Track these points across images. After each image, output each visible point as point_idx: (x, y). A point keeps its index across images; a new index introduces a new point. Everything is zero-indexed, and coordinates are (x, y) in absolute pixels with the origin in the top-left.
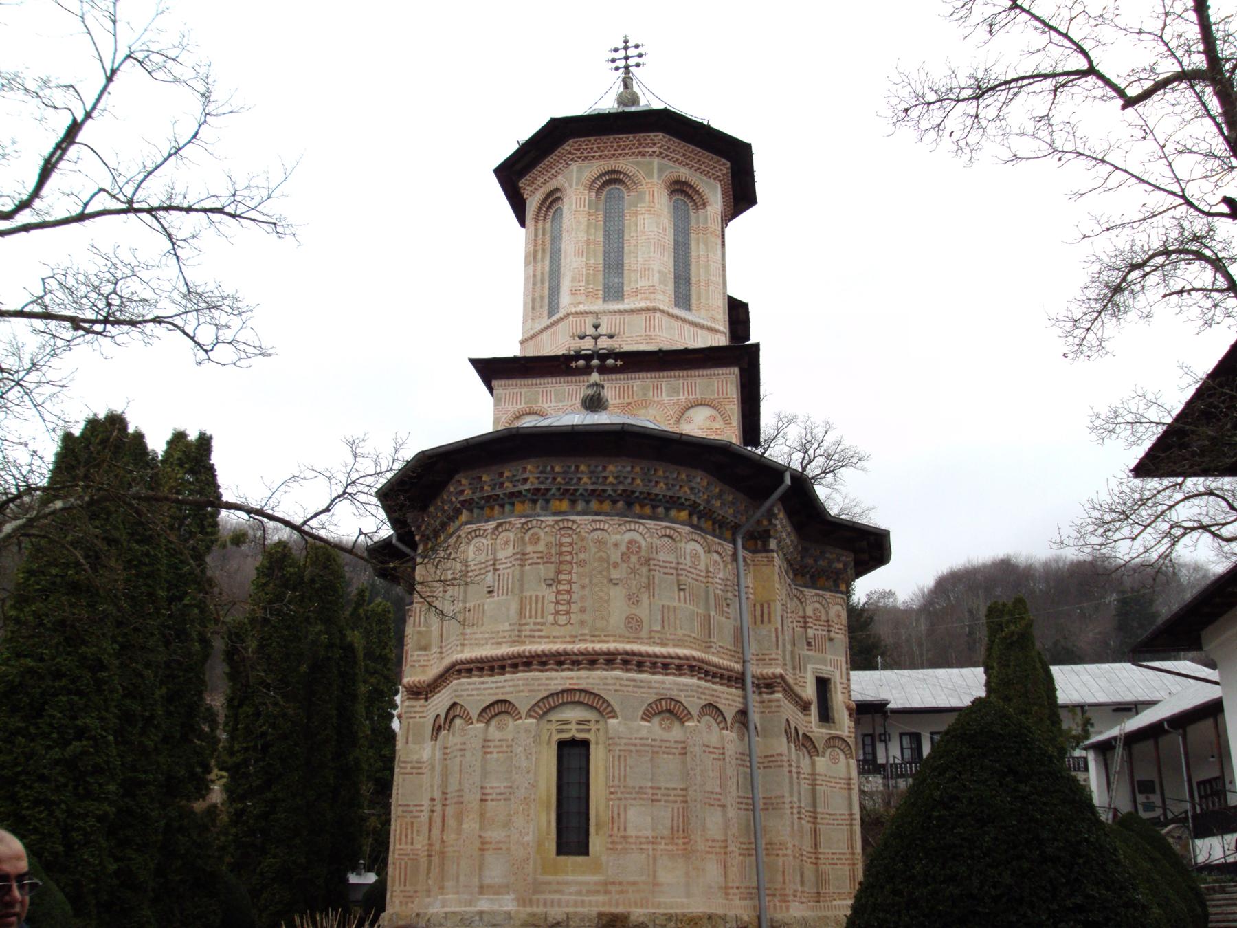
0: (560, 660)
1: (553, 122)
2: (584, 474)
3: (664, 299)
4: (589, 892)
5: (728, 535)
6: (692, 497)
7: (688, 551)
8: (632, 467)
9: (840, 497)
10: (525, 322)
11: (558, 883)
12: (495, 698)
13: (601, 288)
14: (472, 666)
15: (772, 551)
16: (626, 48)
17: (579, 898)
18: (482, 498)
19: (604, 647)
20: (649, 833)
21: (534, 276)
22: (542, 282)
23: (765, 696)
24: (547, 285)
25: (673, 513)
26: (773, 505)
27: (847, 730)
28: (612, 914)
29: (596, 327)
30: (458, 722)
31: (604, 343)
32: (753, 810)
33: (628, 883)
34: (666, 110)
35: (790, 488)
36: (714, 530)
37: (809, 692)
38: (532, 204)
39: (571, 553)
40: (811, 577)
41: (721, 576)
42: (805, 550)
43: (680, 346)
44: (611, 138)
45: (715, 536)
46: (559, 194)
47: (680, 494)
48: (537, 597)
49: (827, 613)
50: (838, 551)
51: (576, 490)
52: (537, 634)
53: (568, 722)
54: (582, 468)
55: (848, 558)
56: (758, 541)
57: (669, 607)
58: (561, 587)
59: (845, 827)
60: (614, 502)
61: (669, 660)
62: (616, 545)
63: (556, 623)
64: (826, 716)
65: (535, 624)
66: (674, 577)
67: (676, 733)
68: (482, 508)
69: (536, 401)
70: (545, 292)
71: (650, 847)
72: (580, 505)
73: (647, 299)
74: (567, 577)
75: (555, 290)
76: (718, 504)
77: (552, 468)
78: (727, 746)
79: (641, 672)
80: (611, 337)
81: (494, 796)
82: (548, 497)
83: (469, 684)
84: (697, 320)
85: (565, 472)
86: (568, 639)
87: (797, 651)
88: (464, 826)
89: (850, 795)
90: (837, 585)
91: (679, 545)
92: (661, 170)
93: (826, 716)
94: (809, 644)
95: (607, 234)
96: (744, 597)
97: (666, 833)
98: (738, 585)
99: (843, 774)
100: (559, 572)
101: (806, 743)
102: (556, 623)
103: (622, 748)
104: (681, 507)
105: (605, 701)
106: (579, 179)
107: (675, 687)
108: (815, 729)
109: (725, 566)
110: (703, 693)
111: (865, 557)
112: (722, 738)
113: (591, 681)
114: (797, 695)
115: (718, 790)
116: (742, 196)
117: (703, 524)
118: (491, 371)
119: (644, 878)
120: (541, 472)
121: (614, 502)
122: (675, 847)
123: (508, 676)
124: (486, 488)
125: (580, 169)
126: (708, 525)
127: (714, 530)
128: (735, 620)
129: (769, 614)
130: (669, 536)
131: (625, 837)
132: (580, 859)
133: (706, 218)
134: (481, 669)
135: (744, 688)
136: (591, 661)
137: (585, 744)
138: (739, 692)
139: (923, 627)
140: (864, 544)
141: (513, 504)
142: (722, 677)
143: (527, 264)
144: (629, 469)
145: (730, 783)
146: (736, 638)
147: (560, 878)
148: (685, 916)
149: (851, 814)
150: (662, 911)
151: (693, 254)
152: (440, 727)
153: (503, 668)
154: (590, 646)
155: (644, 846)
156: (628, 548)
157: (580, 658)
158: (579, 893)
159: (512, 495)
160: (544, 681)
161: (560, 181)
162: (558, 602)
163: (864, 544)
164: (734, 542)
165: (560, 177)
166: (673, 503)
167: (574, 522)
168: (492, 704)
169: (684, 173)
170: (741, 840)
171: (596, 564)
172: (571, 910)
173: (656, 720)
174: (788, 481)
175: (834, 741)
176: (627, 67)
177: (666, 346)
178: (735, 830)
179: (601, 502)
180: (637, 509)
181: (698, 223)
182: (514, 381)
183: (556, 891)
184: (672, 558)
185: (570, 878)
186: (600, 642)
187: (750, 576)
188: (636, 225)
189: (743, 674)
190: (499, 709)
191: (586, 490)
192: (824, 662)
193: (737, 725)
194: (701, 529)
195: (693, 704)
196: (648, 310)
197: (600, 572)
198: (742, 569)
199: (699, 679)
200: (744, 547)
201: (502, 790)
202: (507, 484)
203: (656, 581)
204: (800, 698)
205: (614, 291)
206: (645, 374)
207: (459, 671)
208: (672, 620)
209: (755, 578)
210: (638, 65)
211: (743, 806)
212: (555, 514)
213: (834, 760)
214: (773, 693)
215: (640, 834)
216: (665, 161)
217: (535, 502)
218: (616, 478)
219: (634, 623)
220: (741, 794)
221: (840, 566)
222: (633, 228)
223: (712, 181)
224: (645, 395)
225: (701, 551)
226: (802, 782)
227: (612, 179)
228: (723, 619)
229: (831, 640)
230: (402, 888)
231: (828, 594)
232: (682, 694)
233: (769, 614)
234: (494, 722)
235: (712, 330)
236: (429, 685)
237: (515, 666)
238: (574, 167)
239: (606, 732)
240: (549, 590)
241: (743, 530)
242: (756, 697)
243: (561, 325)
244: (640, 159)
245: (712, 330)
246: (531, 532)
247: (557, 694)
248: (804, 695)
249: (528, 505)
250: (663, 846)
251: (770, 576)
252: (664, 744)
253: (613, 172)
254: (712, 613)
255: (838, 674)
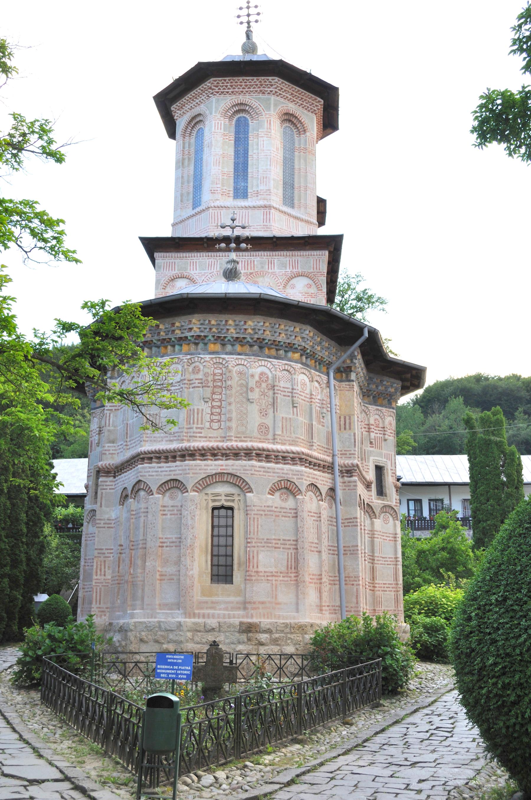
0: (214, 453)
1: (200, 64)
2: (232, 324)
3: (276, 199)
4: (233, 609)
5: (324, 369)
6: (303, 344)
7: (299, 380)
8: (264, 323)
9: (45, 155)
10: (175, 210)
11: (213, 602)
12: (169, 478)
13: (232, 189)
14: (152, 455)
15: (353, 381)
16: (248, 8)
17: (227, 612)
18: (159, 340)
19: (244, 445)
20: (273, 569)
21: (182, 177)
22: (188, 182)
23: (346, 479)
24: (191, 184)
25: (290, 354)
26: (355, 350)
27: (394, 501)
28: (250, 624)
29: (233, 220)
30: (142, 493)
31: (238, 232)
32: (338, 555)
33: (259, 602)
34: (281, 61)
35: (367, 340)
36: (315, 366)
37: (371, 476)
38: (181, 124)
39: (221, 380)
40: (374, 397)
41: (319, 397)
42: (370, 379)
43: (289, 235)
44: (241, 79)
45: (316, 370)
46: (201, 118)
47: (296, 342)
48: (198, 409)
49: (383, 422)
50: (392, 380)
51: (225, 337)
52: (198, 435)
53: (218, 495)
54: (230, 322)
55: (398, 384)
56: (344, 373)
57: (286, 418)
58: (214, 404)
59: (392, 566)
60: (251, 346)
61: (286, 454)
62: (252, 376)
63: (211, 428)
64: (381, 492)
65: (197, 428)
66: (290, 398)
67: (290, 503)
68: (158, 347)
69: (186, 269)
70: (191, 188)
71: (274, 578)
72: (229, 348)
73: (264, 199)
74: (219, 397)
75: (198, 188)
76: (319, 348)
77: (210, 321)
78: (322, 512)
79: (268, 462)
80: (244, 228)
81: (168, 544)
82: (206, 341)
83: (150, 468)
84: (299, 215)
85: (219, 324)
86: (219, 439)
87: (364, 448)
88: (147, 564)
89: (396, 545)
90: (390, 403)
91: (294, 376)
92: (276, 105)
93: (381, 492)
94: (371, 443)
95: (236, 152)
96: (334, 411)
97: (284, 569)
98: (330, 404)
99: (391, 531)
100: (213, 393)
101: (369, 509)
102: (211, 428)
103: (256, 512)
104: (295, 350)
105: (244, 481)
106: (217, 108)
107: (290, 472)
108: (374, 500)
109: (322, 391)
110: (308, 477)
111: (408, 384)
112: (319, 507)
113: (235, 467)
114: (364, 478)
115: (316, 541)
116: (329, 123)
117: (309, 362)
118: (154, 246)
119: (269, 599)
120: (202, 324)
121: (251, 346)
122: (289, 579)
123: (178, 463)
124: (162, 333)
125: (218, 101)
126: (311, 362)
127: (315, 366)
128: (328, 427)
129: (350, 423)
130: (287, 370)
131: (257, 572)
132: (228, 586)
133: (306, 141)
134: (159, 458)
135: (333, 474)
136: (235, 454)
137: (231, 509)
138: (330, 476)
139: (466, 441)
140: (409, 376)
141: (181, 345)
142: (319, 465)
143: (177, 168)
144: (262, 324)
145: (324, 536)
146: (328, 439)
147: (214, 599)
148: (296, 624)
149: (396, 558)
150: (282, 621)
151: (296, 167)
152: (127, 496)
153: (174, 457)
154: (234, 444)
155: (269, 578)
156: (260, 378)
157: (228, 452)
158: (226, 609)
159: (181, 338)
160: (203, 467)
161: (202, 108)
162: (212, 414)
163: (409, 376)
164: (328, 374)
165: (202, 106)
166: (290, 347)
167: (224, 359)
168: (167, 482)
169: (292, 108)
170: (330, 574)
171: (239, 388)
172: (221, 620)
173: (277, 494)
174: (366, 334)
175: (387, 509)
176: (248, 23)
177: (278, 234)
178: (326, 568)
179: (242, 346)
180: (266, 351)
181: (300, 144)
182: (170, 254)
183: (211, 608)
184: (289, 385)
185: (220, 599)
186: (241, 441)
187: (338, 397)
188: (258, 145)
189: (333, 463)
190: (174, 485)
191: (232, 337)
192: (380, 455)
193: (328, 498)
194: (307, 366)
195: (303, 485)
196: (265, 207)
197: (241, 394)
198: (333, 392)
199: (306, 467)
200: (334, 378)
201: (174, 540)
202: (177, 331)
203: (279, 401)
204: (366, 479)
205: (241, 192)
206: (262, 253)
207: (143, 459)
208: (288, 427)
209: (340, 398)
210: (257, 21)
211: (331, 552)
212: (210, 353)
213: (386, 521)
214: (351, 476)
215: (267, 570)
216: (278, 98)
217: (197, 344)
218: (254, 329)
219: (263, 429)
220: (331, 544)
221: (393, 390)
222: (255, 147)
223: (310, 114)
224: (262, 267)
225: (307, 380)
226: (366, 535)
227: (241, 109)
228: (320, 427)
229: (385, 440)
230: (98, 605)
231: (384, 409)
232: (295, 477)
233: (350, 423)
234: (168, 494)
235: (307, 222)
236: (117, 467)
237: (183, 456)
238: (213, 99)
239: (245, 501)
240: (206, 405)
241: (334, 367)
242: (341, 480)
243: (203, 215)
244: (261, 95)
245: (307, 222)
246: (193, 365)
247: (212, 476)
248: (368, 478)
249: (193, 347)
250: (281, 578)
251: (350, 397)
252: (283, 511)
253: (241, 104)
254: (314, 423)
255: (389, 463)
